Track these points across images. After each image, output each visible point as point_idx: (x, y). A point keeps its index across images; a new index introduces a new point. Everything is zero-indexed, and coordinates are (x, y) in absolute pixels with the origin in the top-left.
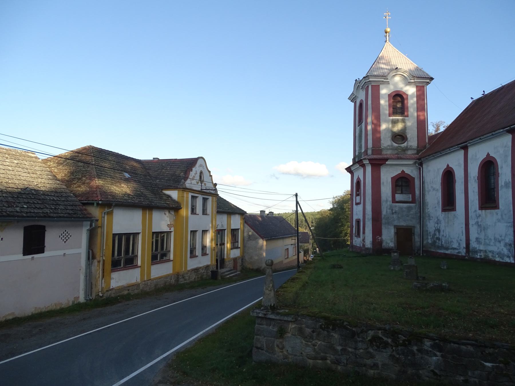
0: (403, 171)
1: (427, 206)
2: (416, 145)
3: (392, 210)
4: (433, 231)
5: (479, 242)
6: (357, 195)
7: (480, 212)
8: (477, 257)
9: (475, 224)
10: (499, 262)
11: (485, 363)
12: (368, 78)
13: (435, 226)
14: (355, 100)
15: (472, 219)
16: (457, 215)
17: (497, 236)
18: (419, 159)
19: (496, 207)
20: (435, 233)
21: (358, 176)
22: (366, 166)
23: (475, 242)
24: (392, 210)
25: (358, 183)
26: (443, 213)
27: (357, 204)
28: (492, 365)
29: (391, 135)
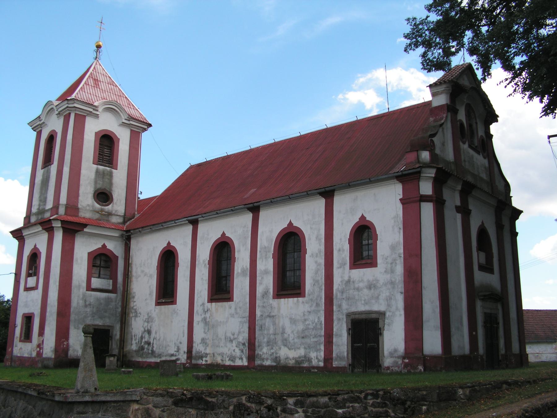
0: (104, 246)
1: (134, 297)
2: (123, 211)
5: (206, 344)
6: (29, 275)
8: (202, 363)
9: (202, 320)
10: (230, 366)
11: (337, 411)
12: (73, 102)
13: (144, 326)
14: (40, 129)
16: (178, 310)
17: (229, 335)
18: (127, 231)
19: (230, 299)
20: (144, 336)
23: (200, 343)
24: (85, 301)
25: (34, 256)
26: (158, 307)
28: (343, 411)
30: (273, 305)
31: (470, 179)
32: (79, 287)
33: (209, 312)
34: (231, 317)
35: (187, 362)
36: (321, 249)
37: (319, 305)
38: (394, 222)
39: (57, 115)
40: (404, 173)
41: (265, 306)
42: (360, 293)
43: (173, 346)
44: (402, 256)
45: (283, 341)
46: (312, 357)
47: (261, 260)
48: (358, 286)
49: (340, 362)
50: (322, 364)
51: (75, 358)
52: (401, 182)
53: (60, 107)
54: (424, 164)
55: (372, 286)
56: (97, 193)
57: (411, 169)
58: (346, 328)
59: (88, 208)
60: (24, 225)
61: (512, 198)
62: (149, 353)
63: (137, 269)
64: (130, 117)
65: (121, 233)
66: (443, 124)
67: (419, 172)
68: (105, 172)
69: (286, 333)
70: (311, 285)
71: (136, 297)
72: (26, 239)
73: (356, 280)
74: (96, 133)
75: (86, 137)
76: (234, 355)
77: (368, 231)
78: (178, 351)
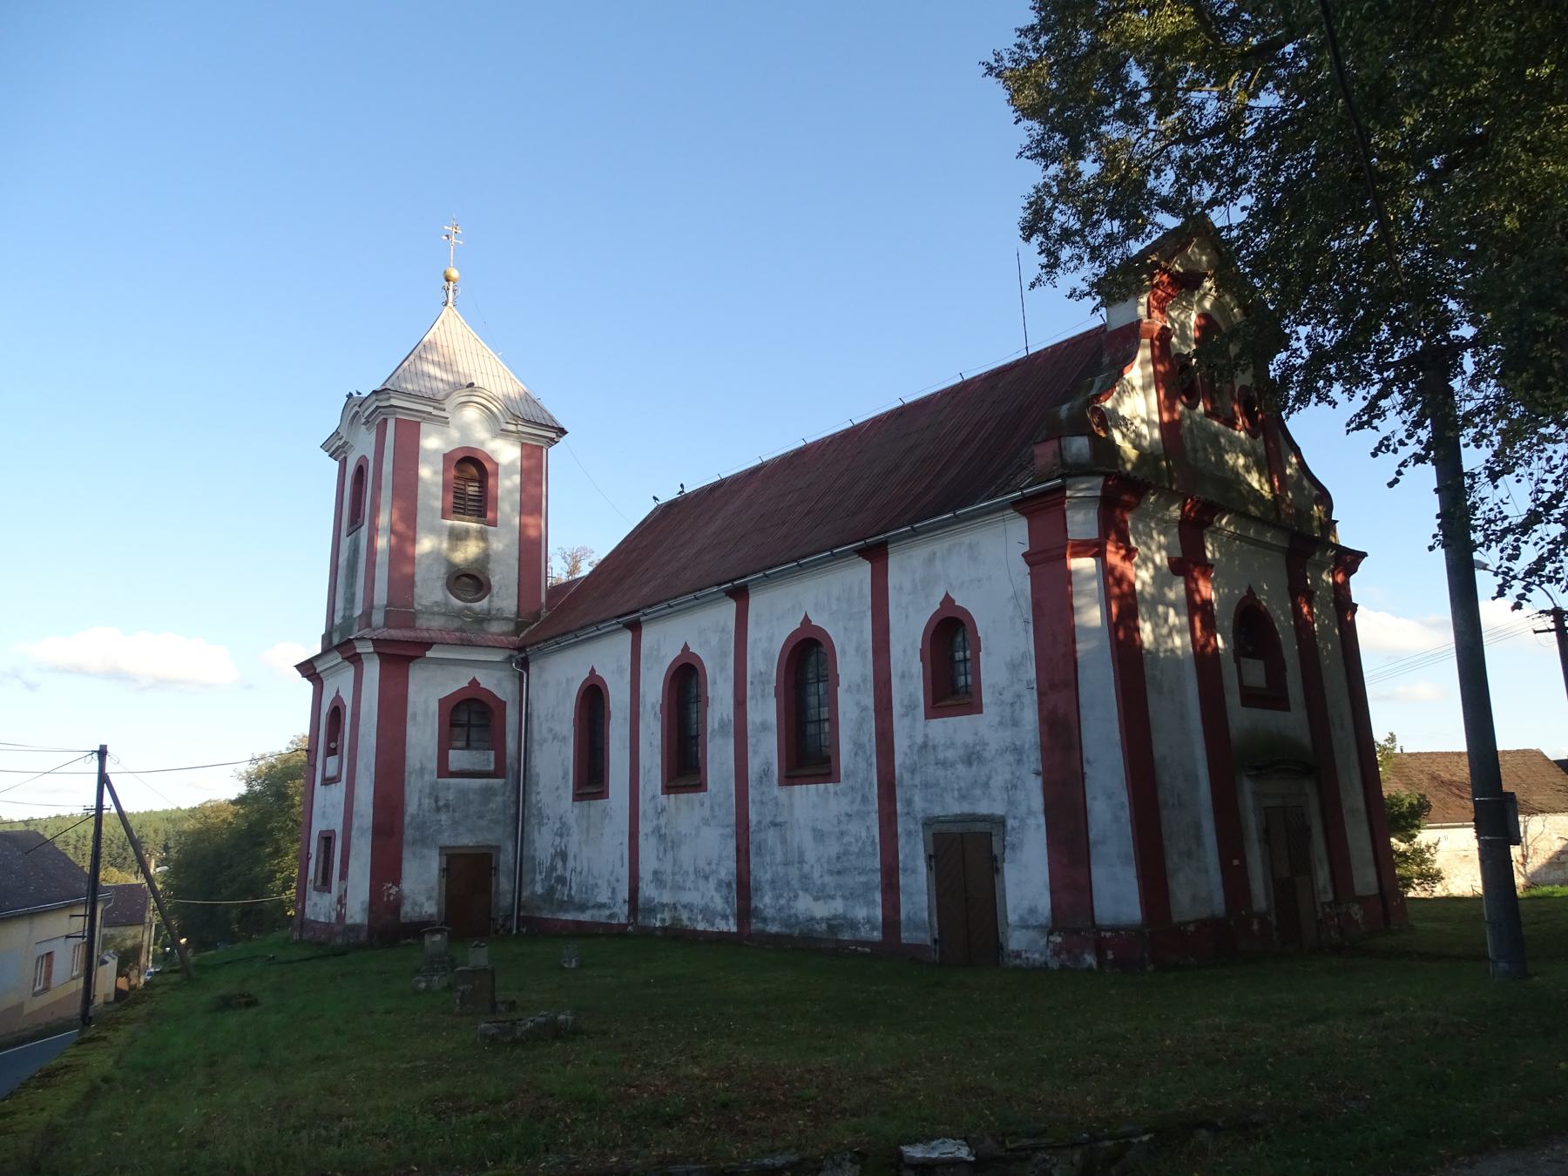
0: (474, 683)
1: (537, 784)
2: (514, 609)
3: (437, 800)
6: (331, 752)
9: (653, 832)
10: (704, 932)
14: (343, 455)
17: (702, 864)
18: (521, 649)
19: (700, 786)
21: (338, 691)
22: (365, 665)
23: (652, 882)
24: (437, 800)
25: (336, 713)
26: (577, 803)
27: (327, 781)
29: (445, 574)
34: (705, 824)
43: (606, 883)
47: (754, 700)
49: (914, 934)
50: (877, 935)
51: (417, 920)
53: (367, 409)
55: (974, 757)
61: (1337, 524)
63: (540, 725)
65: (507, 653)
67: (1062, 489)
69: (807, 863)
73: (939, 743)
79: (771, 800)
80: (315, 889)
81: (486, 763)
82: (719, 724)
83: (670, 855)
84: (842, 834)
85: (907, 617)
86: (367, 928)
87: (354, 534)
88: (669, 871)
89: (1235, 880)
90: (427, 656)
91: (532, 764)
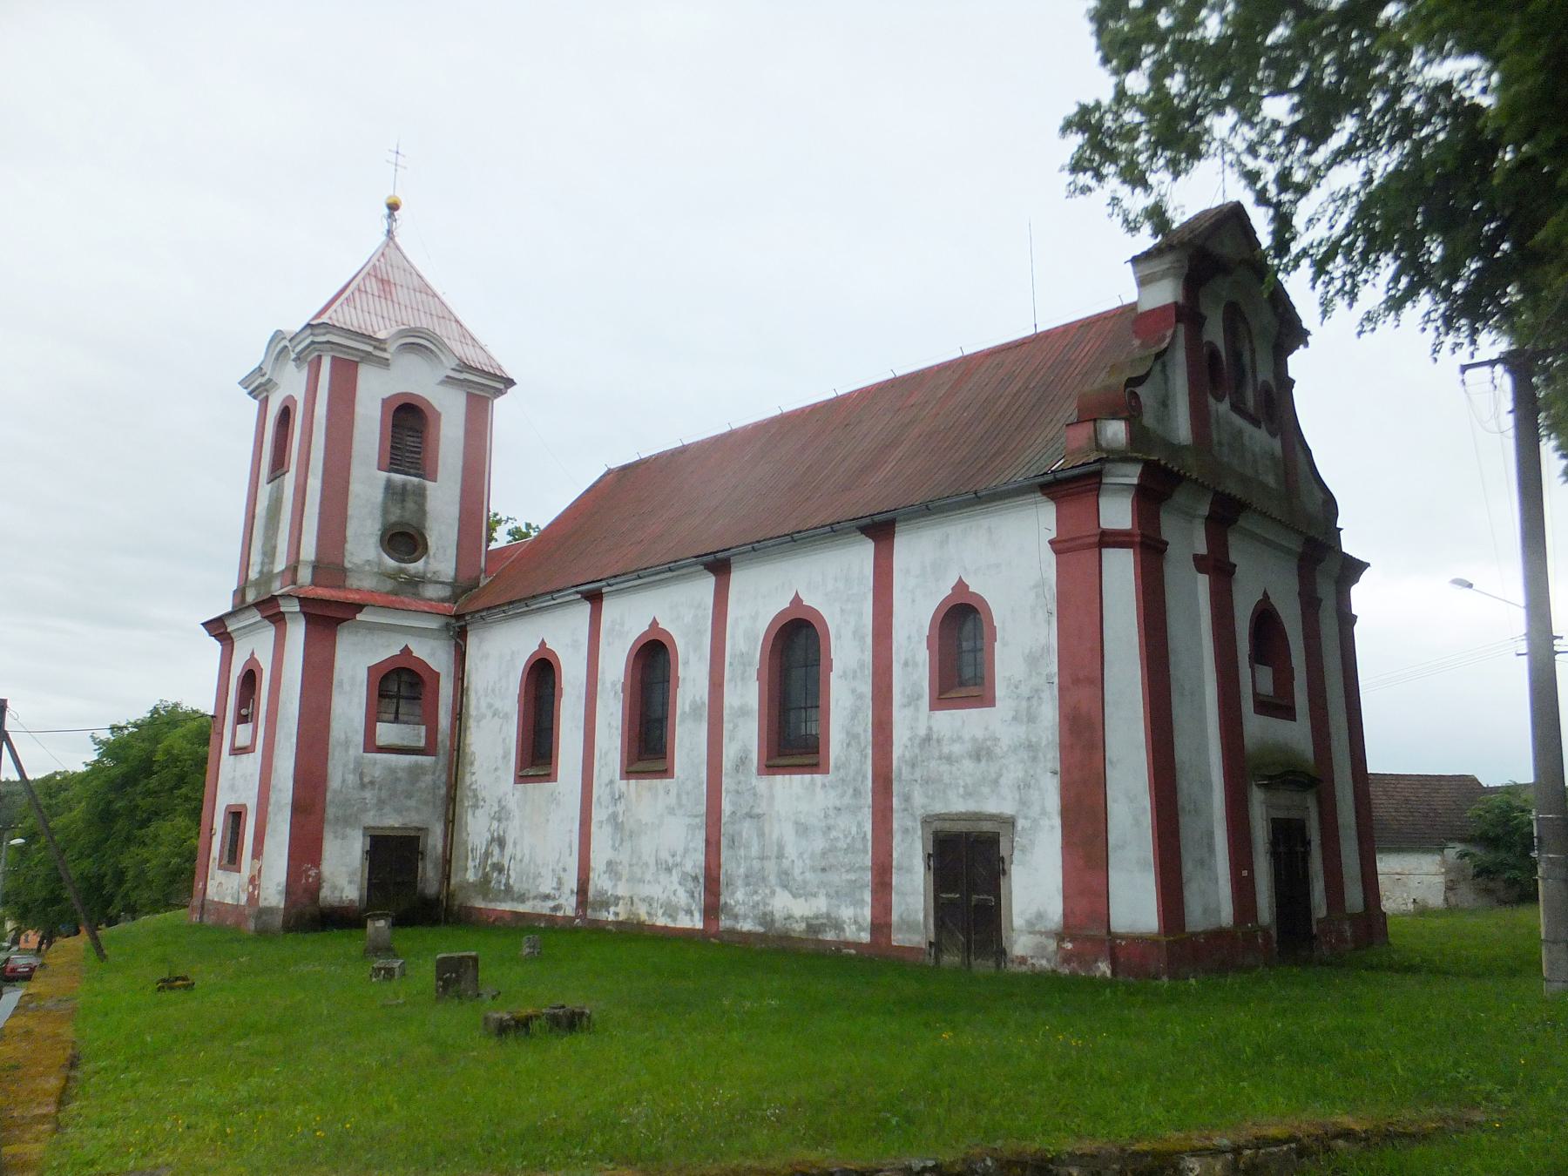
0: (406, 651)
1: (472, 764)
2: (452, 573)
3: (361, 776)
4: (485, 843)
5: (616, 874)
6: (242, 719)
7: (622, 785)
9: (608, 820)
13: (492, 829)
14: (265, 394)
15: (601, 807)
16: (559, 793)
17: (665, 855)
18: (458, 617)
19: (666, 773)
21: (253, 653)
22: (288, 625)
23: (605, 873)
24: (361, 776)
25: (250, 679)
26: (520, 786)
27: (237, 751)
29: (379, 530)
30: (758, 790)
31: (1233, 488)
32: (347, 744)
33: (622, 800)
34: (670, 813)
35: (577, 914)
36: (864, 661)
37: (860, 793)
38: (1037, 596)
39: (294, 360)
40: (1059, 476)
41: (740, 791)
42: (954, 769)
43: (551, 874)
44: (1056, 680)
45: (779, 876)
46: (845, 918)
48: (950, 751)
50: (865, 937)
51: (336, 904)
52: (1053, 497)
54: (1110, 451)
55: (984, 753)
56: (387, 538)
57: (1078, 466)
58: (922, 853)
59: (367, 568)
60: (233, 607)
61: (1341, 532)
62: (500, 891)
63: (478, 699)
64: (462, 364)
66: (1165, 350)
67: (1098, 475)
68: (408, 488)
69: (787, 858)
70: (842, 745)
71: (476, 763)
72: (235, 640)
74: (383, 399)
75: (360, 410)
76: (674, 903)
77: (975, 618)
78: (559, 889)
79: (748, 790)
80: (220, 867)
81: (416, 738)
82: (690, 706)
83: (627, 845)
84: (829, 829)
85: (913, 601)
86: (282, 912)
87: (277, 481)
88: (625, 863)
89: (1243, 889)
90: (358, 619)
91: (467, 742)
